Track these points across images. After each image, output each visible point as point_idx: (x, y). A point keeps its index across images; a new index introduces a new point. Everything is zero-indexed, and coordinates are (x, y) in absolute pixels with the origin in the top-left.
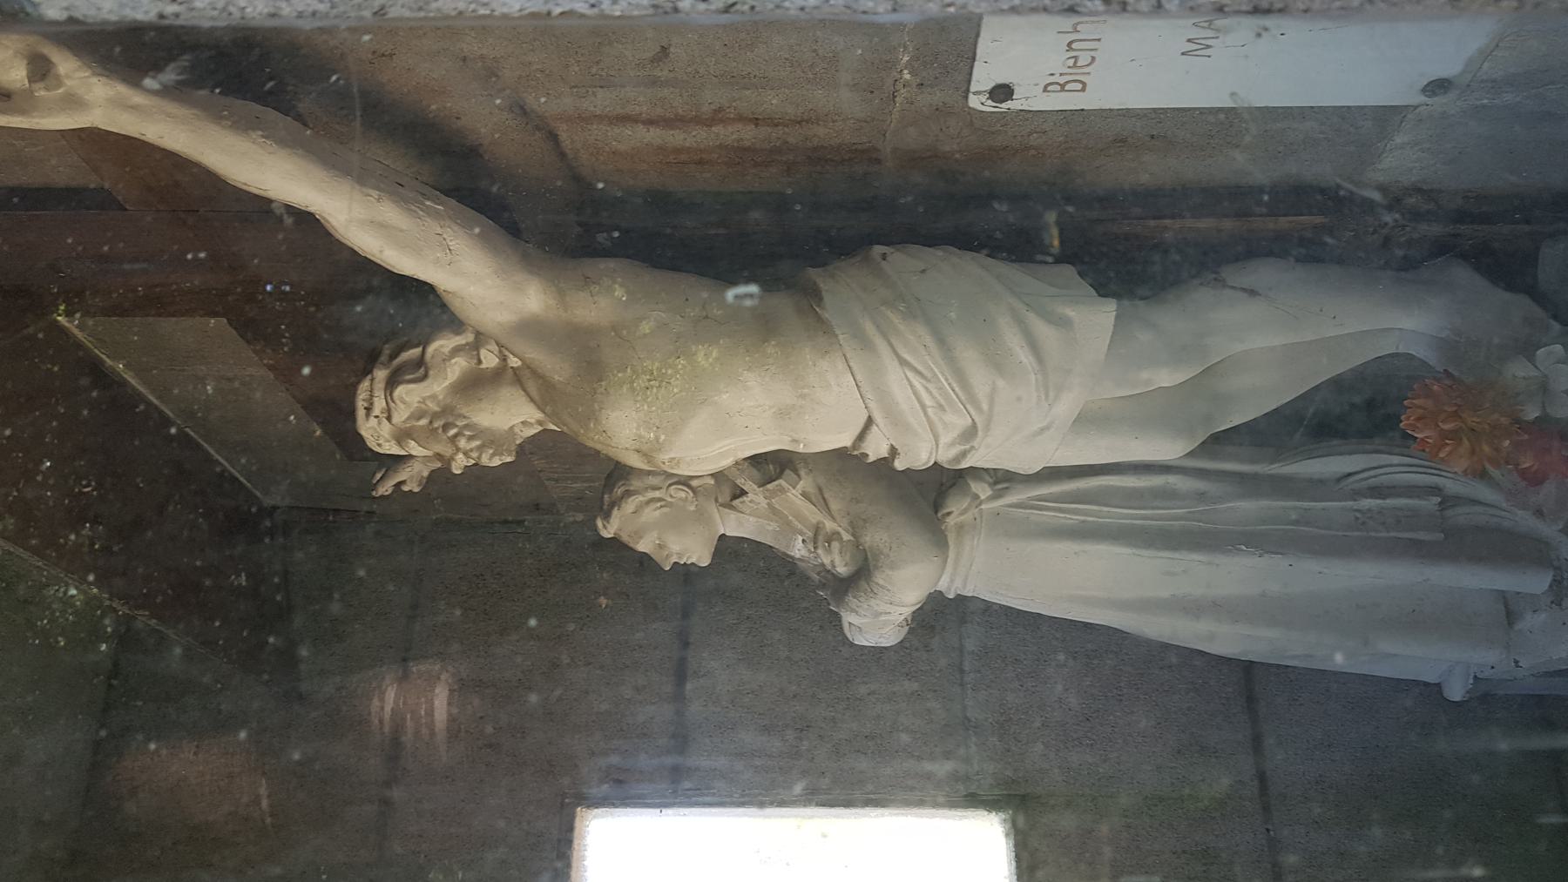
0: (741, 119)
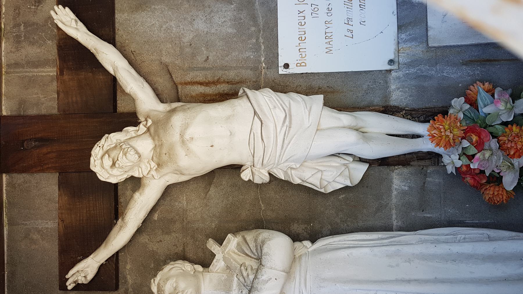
0: (224, 82)
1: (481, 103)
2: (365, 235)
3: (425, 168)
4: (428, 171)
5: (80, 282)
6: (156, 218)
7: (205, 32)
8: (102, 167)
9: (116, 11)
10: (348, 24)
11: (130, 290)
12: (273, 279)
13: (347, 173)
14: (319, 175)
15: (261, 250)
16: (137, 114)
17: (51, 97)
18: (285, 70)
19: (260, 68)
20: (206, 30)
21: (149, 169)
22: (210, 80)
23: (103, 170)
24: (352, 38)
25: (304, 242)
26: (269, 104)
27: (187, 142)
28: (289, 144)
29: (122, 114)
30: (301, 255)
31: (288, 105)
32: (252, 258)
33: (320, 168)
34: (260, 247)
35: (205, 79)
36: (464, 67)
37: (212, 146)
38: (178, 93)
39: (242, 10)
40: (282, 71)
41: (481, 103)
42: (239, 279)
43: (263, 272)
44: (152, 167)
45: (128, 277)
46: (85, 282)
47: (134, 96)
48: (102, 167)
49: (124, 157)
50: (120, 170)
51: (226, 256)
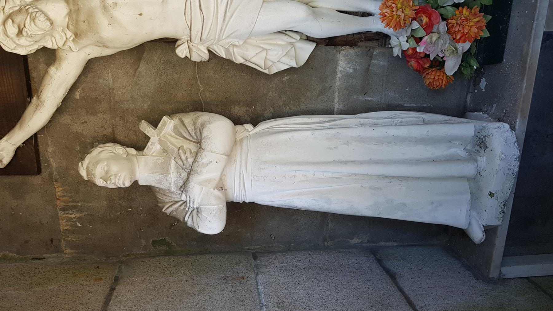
2: (307, 119)
4: (374, 53)
6: (78, 97)
11: (55, 173)
13: (293, 53)
15: (201, 133)
21: (65, 39)
23: (8, 39)
27: (110, 8)
30: (242, 139)
32: (191, 141)
34: (200, 130)
37: (141, 15)
43: (203, 156)
44: (68, 37)
45: (51, 160)
49: (32, 23)
51: (162, 139)
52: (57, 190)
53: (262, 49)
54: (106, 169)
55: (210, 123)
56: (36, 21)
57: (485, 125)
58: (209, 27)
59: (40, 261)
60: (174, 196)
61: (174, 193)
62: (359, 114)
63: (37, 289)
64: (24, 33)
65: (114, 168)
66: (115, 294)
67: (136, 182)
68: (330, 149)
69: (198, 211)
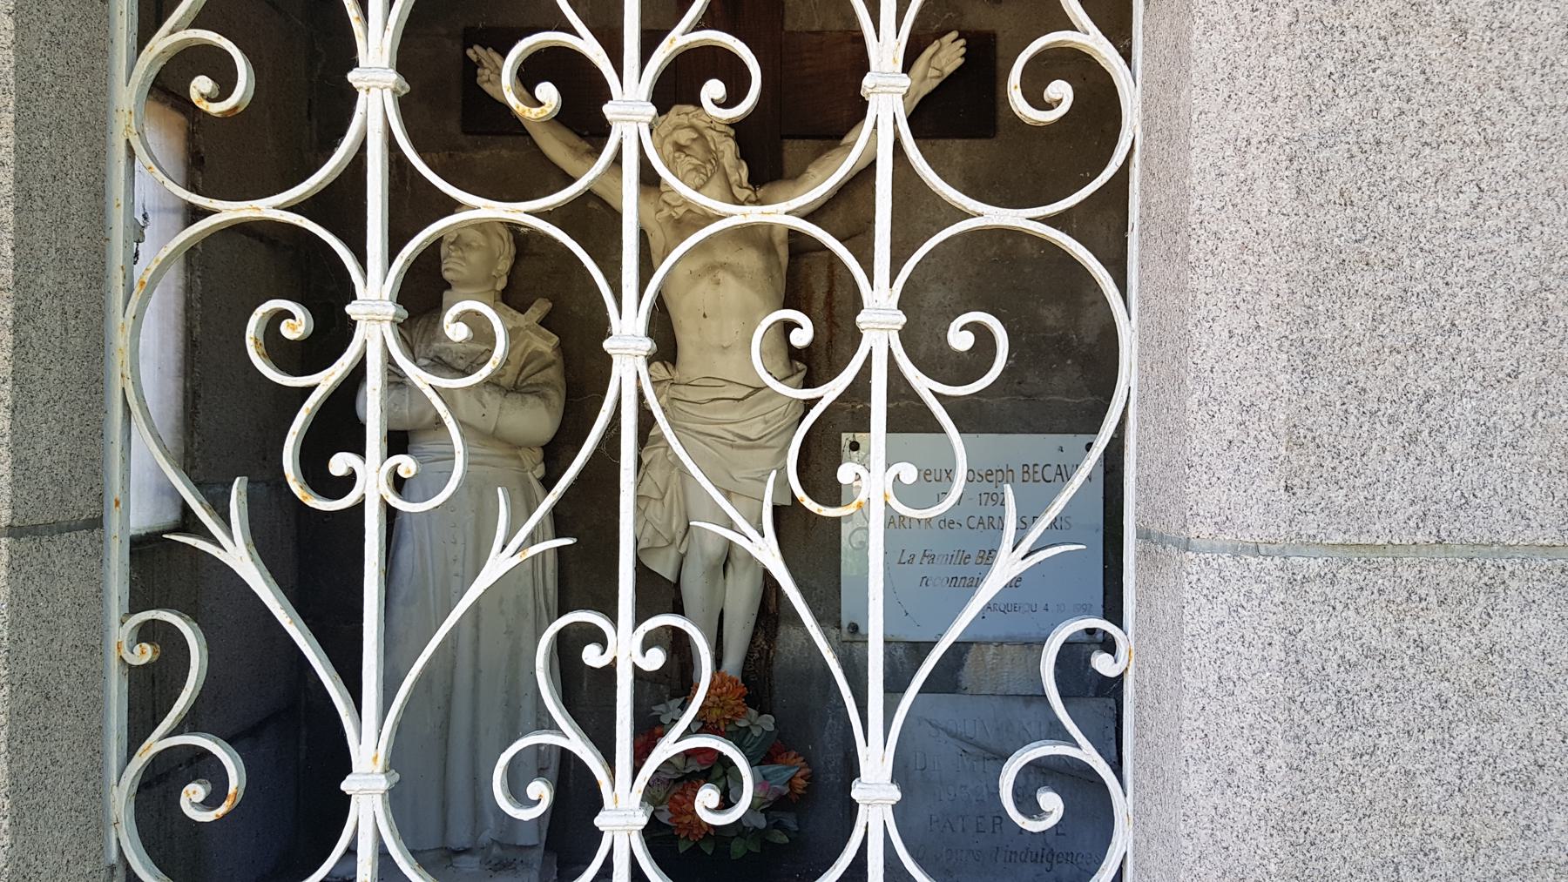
0: (832, 335)
1: (771, 769)
2: (552, 567)
3: (667, 680)
4: (662, 686)
5: (480, 71)
6: (590, 205)
7: (921, 303)
8: (678, 127)
9: (966, 141)
10: (924, 556)
11: (464, 156)
12: (484, 411)
13: (661, 543)
14: (656, 495)
15: (530, 393)
16: (768, 185)
17: (815, 15)
18: (848, 443)
19: (856, 399)
20: (926, 305)
21: (674, 204)
22: (837, 309)
23: (671, 128)
24: (900, 563)
25: (543, 465)
26: (773, 413)
27: (711, 275)
28: (705, 444)
29: (779, 152)
30: (521, 459)
31: (768, 444)
32: (518, 377)
33: (668, 497)
34: (537, 391)
35: (837, 299)
36: (841, 755)
37: (705, 316)
38: (815, 251)
39: (958, 370)
40: (846, 438)
41: (771, 769)
42: (482, 354)
43: (494, 395)
44: (676, 210)
45: (487, 153)
46: (479, 80)
47: (801, 179)
48: (678, 127)
49: (690, 167)
50: (671, 157)
51: (521, 333)
52: (434, 154)
53: (662, 490)
54: (474, 244)
55: (547, 408)
56: (694, 173)
57: (535, 866)
58: (691, 411)
59: (305, 114)
60: (423, 346)
61: (429, 344)
62: (548, 837)
63: (267, 115)
64: (677, 155)
65: (474, 257)
66: (255, 242)
67: (448, 286)
68: (501, 601)
69: (398, 383)
